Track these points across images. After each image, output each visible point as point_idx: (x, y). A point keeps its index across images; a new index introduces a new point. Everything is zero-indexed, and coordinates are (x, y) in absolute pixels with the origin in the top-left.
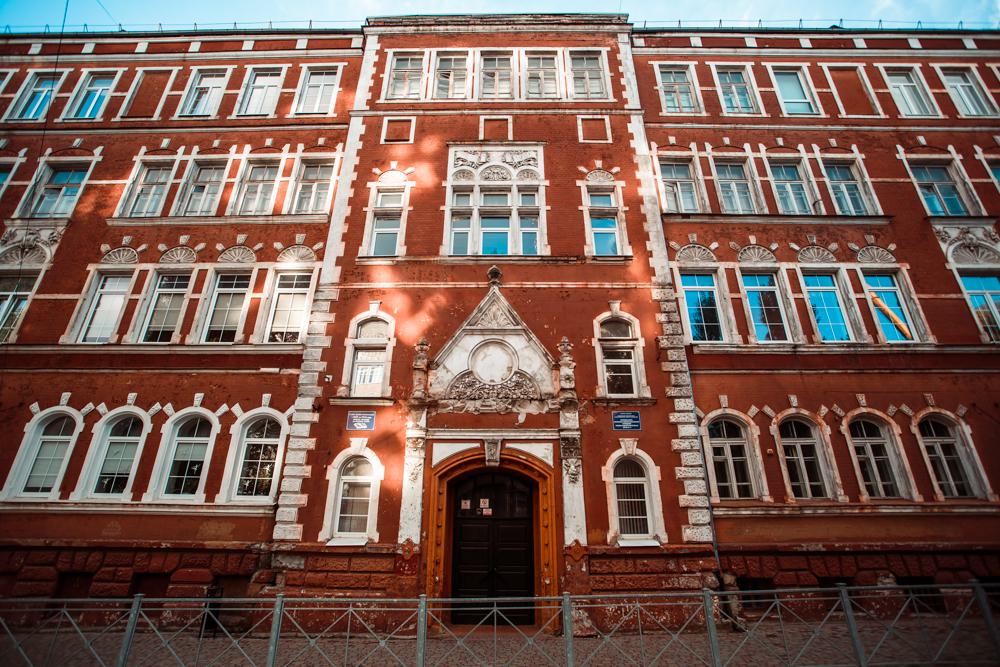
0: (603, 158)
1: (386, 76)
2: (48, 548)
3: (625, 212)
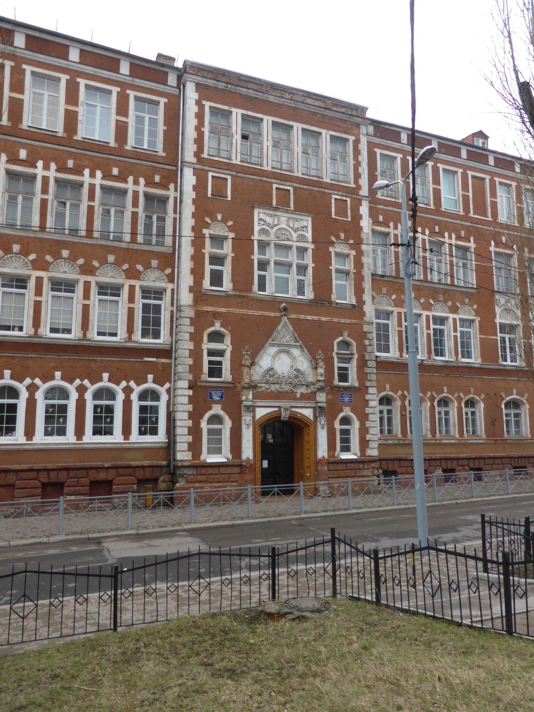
0: (345, 232)
1: (206, 130)
2: (31, 470)
3: (354, 273)
